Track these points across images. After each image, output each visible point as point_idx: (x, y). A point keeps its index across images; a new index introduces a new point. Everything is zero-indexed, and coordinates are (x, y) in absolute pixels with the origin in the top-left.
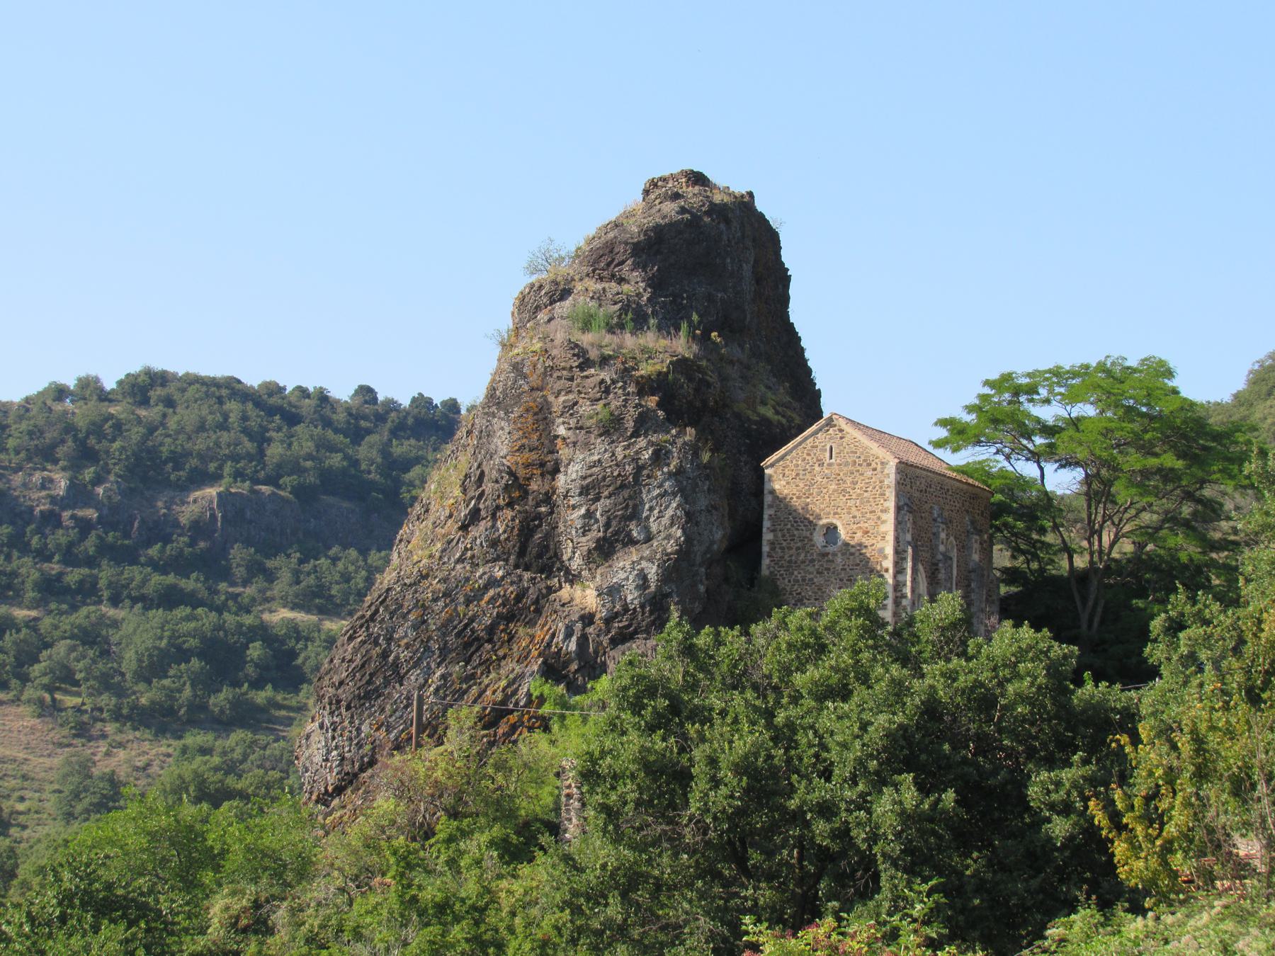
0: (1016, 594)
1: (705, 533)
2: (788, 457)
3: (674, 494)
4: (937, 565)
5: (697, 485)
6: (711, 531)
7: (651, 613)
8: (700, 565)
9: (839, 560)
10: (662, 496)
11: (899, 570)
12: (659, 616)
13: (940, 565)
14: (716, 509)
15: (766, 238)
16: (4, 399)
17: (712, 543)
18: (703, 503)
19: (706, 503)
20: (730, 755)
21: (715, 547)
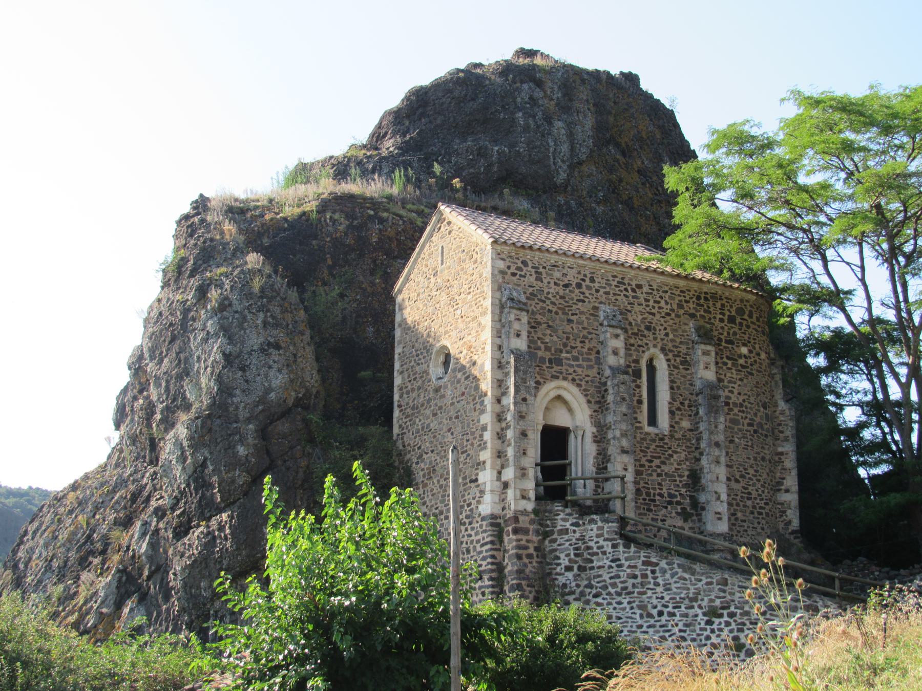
0: (886, 474)
1: (258, 379)
2: (412, 276)
3: (216, 335)
4: (605, 384)
5: (245, 318)
6: (266, 376)
7: (196, 490)
8: (249, 420)
9: (449, 393)
10: (206, 340)
11: (500, 384)
12: (203, 494)
13: (609, 383)
14: (277, 347)
15: (638, 79)
16: (13, 483)
17: (268, 390)
18: (255, 340)
19: (261, 340)
20: (216, 625)
21: (272, 395)
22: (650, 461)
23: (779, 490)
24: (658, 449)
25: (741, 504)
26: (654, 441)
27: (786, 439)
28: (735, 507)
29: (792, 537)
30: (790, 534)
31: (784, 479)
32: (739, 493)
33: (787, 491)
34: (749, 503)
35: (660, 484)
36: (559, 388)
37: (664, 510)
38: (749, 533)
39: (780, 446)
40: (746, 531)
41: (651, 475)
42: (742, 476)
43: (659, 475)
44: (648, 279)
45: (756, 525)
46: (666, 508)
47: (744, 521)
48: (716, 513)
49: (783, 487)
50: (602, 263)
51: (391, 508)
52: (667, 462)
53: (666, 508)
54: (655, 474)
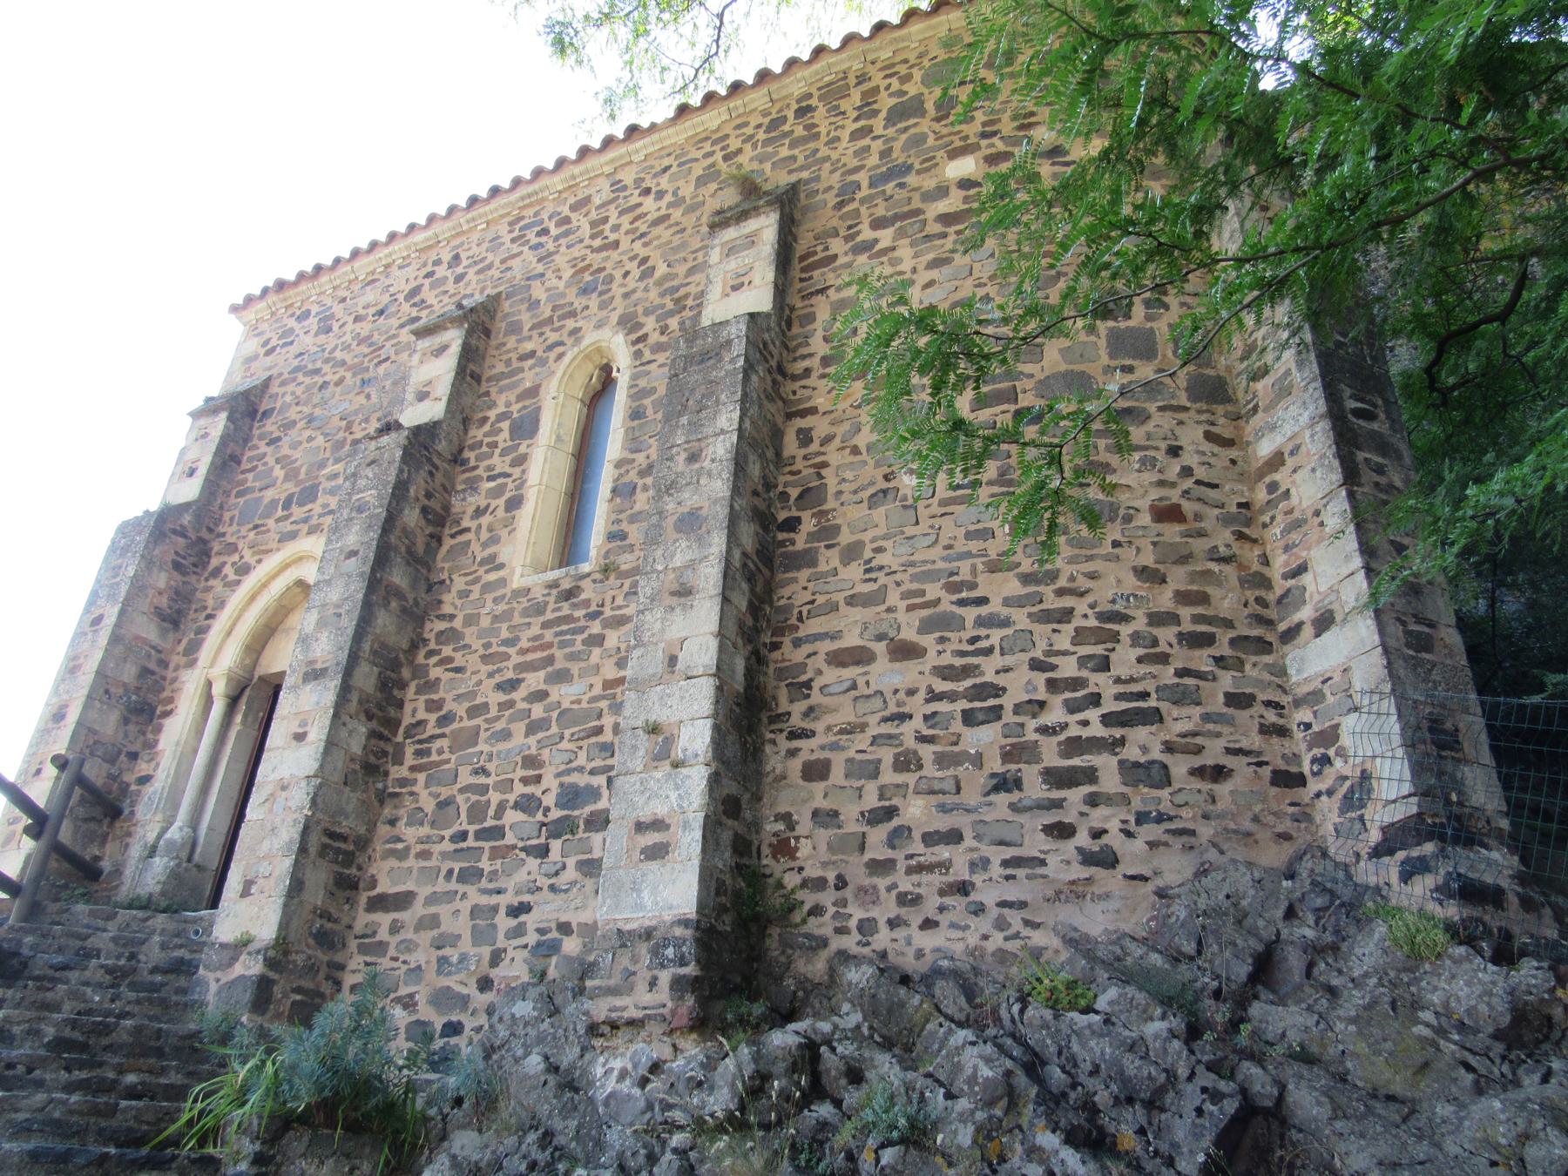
22: (512, 685)
23: (1291, 634)
24: (549, 635)
25: (927, 752)
26: (540, 609)
27: (1284, 391)
28: (888, 777)
29: (1390, 868)
30: (1378, 852)
31: (1302, 569)
32: (918, 706)
33: (1324, 622)
34: (985, 738)
35: (531, 761)
36: (285, 567)
37: (533, 863)
38: (988, 895)
39: (1259, 433)
40: (963, 888)
41: (506, 735)
42: (940, 624)
43: (532, 729)
44: (608, 169)
45: (1036, 843)
46: (543, 851)
47: (954, 837)
48: (640, 827)
49: (1306, 613)
50: (488, 201)
51: (610, 977)
52: (575, 668)
53: (543, 851)
54: (519, 728)
